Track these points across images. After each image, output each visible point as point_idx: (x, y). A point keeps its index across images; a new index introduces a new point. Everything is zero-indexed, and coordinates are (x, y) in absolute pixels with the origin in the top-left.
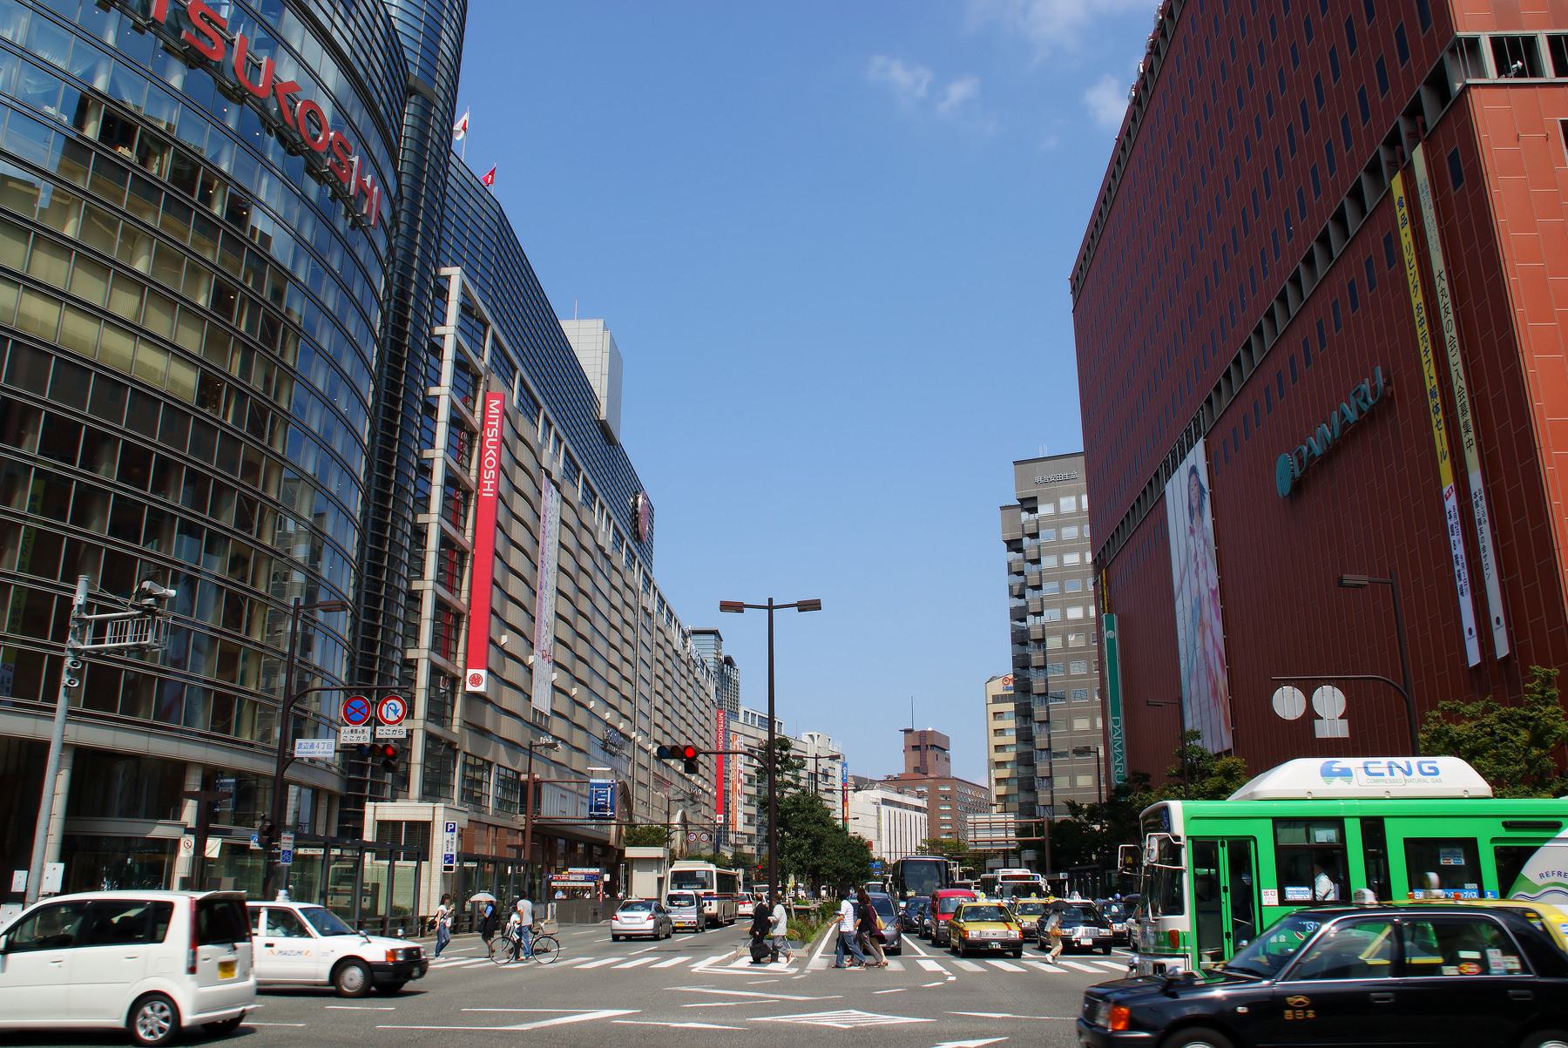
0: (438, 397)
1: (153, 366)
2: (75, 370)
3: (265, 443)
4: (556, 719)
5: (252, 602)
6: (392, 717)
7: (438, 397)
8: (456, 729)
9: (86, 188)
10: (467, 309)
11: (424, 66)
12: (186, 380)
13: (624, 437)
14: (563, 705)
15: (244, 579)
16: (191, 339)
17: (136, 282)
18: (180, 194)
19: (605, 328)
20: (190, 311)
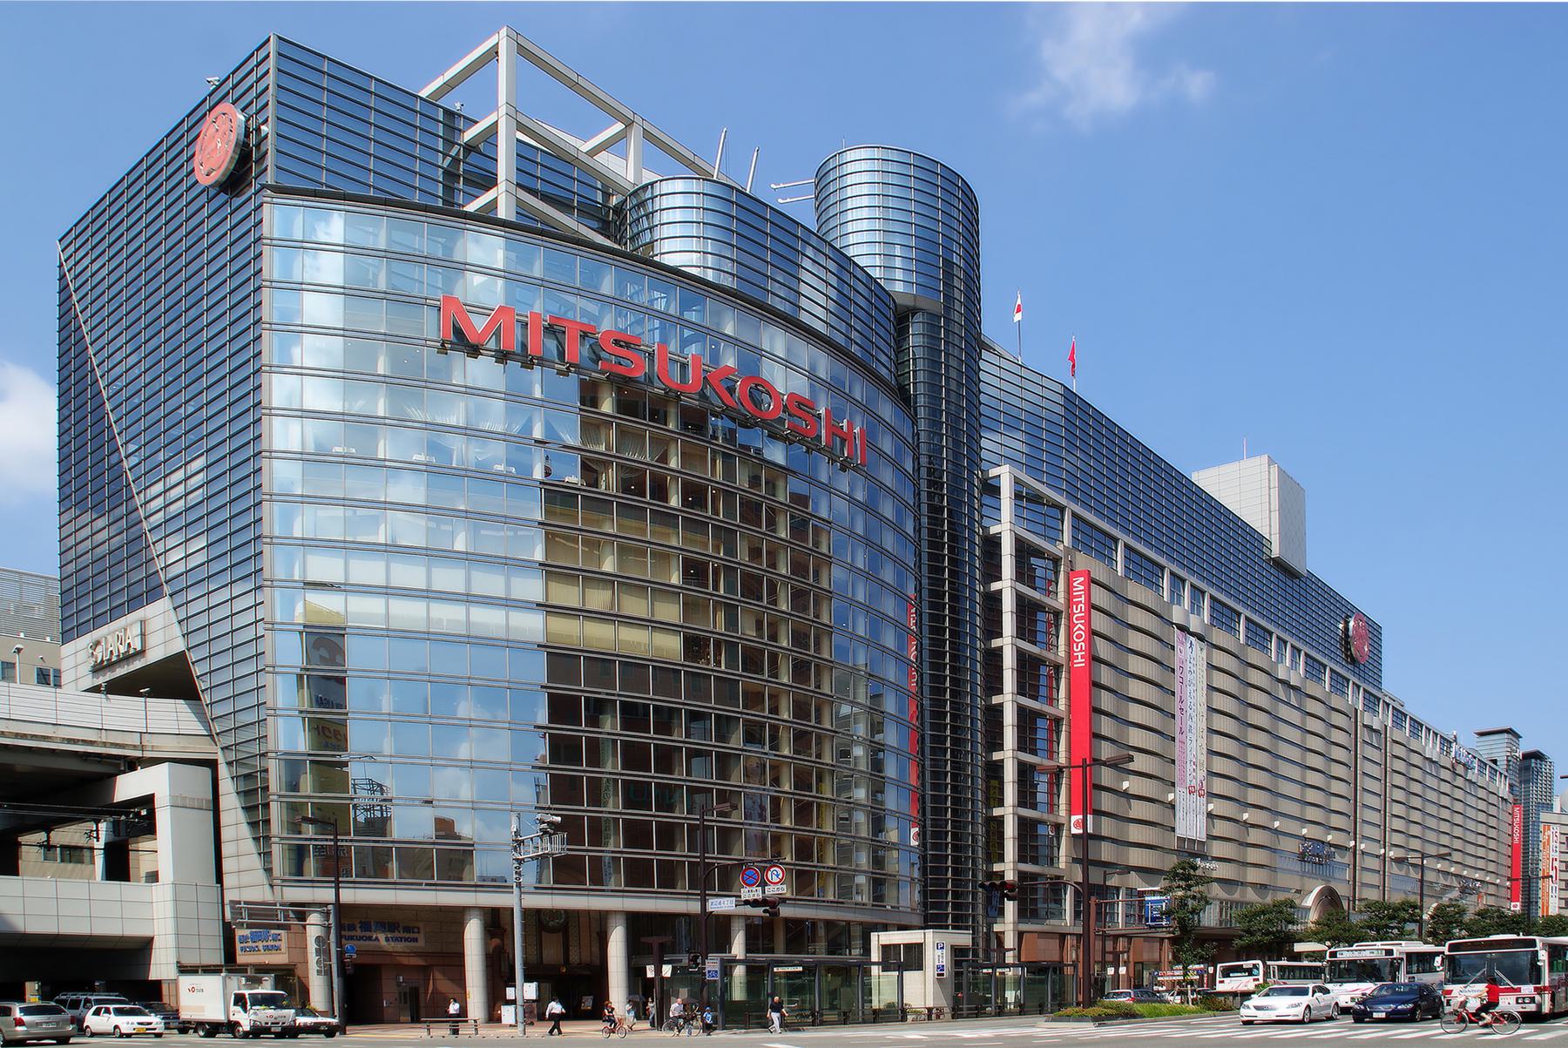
0: (1000, 591)
1: (635, 641)
5: (819, 805)
6: (775, 880)
7: (1000, 591)
9: (614, 531)
10: (1023, 496)
11: (921, 280)
12: (671, 646)
16: (670, 612)
17: (606, 580)
18: (633, 500)
19: (1271, 462)
20: (663, 591)
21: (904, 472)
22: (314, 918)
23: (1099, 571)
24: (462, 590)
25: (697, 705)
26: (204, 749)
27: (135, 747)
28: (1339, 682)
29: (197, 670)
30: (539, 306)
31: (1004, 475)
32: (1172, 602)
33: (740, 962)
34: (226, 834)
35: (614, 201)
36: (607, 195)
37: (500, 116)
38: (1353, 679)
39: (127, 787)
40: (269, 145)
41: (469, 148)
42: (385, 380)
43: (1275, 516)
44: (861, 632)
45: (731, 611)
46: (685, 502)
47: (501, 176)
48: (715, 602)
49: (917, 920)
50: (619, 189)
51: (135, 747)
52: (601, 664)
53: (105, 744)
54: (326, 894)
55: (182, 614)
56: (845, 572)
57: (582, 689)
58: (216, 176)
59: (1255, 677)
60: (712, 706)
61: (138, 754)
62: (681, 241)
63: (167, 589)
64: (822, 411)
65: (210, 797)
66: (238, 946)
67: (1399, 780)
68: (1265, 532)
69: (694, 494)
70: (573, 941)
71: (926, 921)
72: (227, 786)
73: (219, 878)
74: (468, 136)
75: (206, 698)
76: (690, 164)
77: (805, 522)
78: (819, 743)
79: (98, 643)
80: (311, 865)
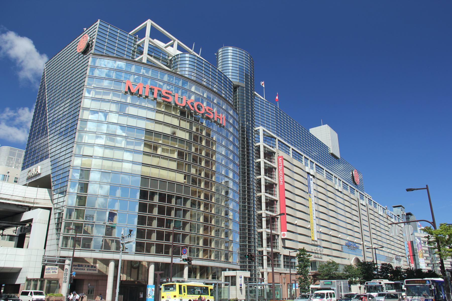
2: (163, 181)
22: (67, 262)
23: (285, 156)
24: (132, 160)
25: (179, 194)
26: (50, 205)
28: (352, 190)
29: (52, 180)
31: (261, 129)
32: (305, 165)
35: (171, 58)
36: (168, 57)
38: (356, 189)
39: (26, 216)
41: (139, 46)
44: (223, 173)
45: (189, 165)
48: (186, 164)
49: (238, 267)
50: (171, 56)
52: (154, 180)
53: (24, 202)
54: (70, 254)
55: (53, 162)
57: (149, 188)
58: (81, 50)
61: (32, 205)
63: (50, 156)
66: (45, 271)
70: (140, 272)
73: (45, 248)
75: (53, 188)
78: (211, 207)
79: (30, 171)
80: (70, 242)
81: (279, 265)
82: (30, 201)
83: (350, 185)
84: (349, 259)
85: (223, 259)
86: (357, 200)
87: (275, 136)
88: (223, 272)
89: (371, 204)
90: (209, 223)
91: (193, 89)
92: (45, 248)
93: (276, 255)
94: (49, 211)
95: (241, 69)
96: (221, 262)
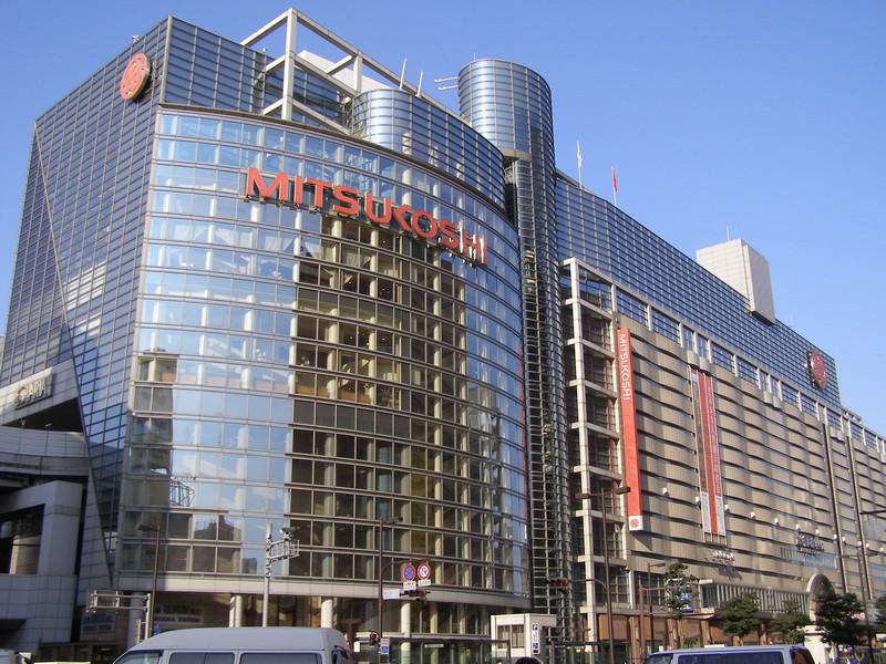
0: (580, 473)
3: (456, 502)
4: (733, 537)
8: (625, 557)
13: (782, 314)
14: (736, 525)
15: (455, 583)
19: (743, 243)
21: (513, 310)
25: (384, 437)
27: (36, 467)
29: (86, 410)
30: (301, 173)
33: (406, 640)
34: (87, 535)
35: (347, 100)
37: (286, 58)
38: (818, 400)
39: (30, 497)
40: (162, 78)
42: (219, 169)
43: (750, 281)
46: (380, 243)
47: (285, 92)
49: (526, 605)
51: (36, 467)
53: (18, 466)
56: (471, 311)
57: (314, 427)
58: (131, 94)
59: (748, 402)
60: (392, 437)
61: (37, 472)
62: (378, 128)
64: (461, 230)
65: (79, 505)
66: (83, 626)
67: (864, 482)
68: (744, 293)
69: (386, 288)
71: (533, 604)
72: (91, 498)
73: (77, 571)
74: (269, 67)
76: (388, 77)
77: (451, 457)
78: (457, 359)
81: (623, 598)
82: (33, 464)
83: (801, 389)
84: (799, 578)
85: (489, 584)
86: (821, 429)
87: (609, 278)
88: (493, 617)
89: (859, 438)
90: (456, 502)
91: (406, 178)
92: (77, 571)
93: (618, 571)
94: (78, 487)
95: (520, 115)
96: (462, 589)
